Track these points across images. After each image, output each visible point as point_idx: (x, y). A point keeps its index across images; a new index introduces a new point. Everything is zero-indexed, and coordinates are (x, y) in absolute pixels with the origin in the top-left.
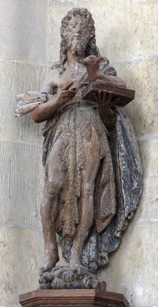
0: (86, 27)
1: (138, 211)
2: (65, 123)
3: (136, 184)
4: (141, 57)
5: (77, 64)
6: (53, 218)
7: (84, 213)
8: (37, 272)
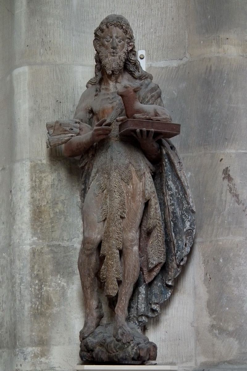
0: (123, 40)
3: (188, 224)
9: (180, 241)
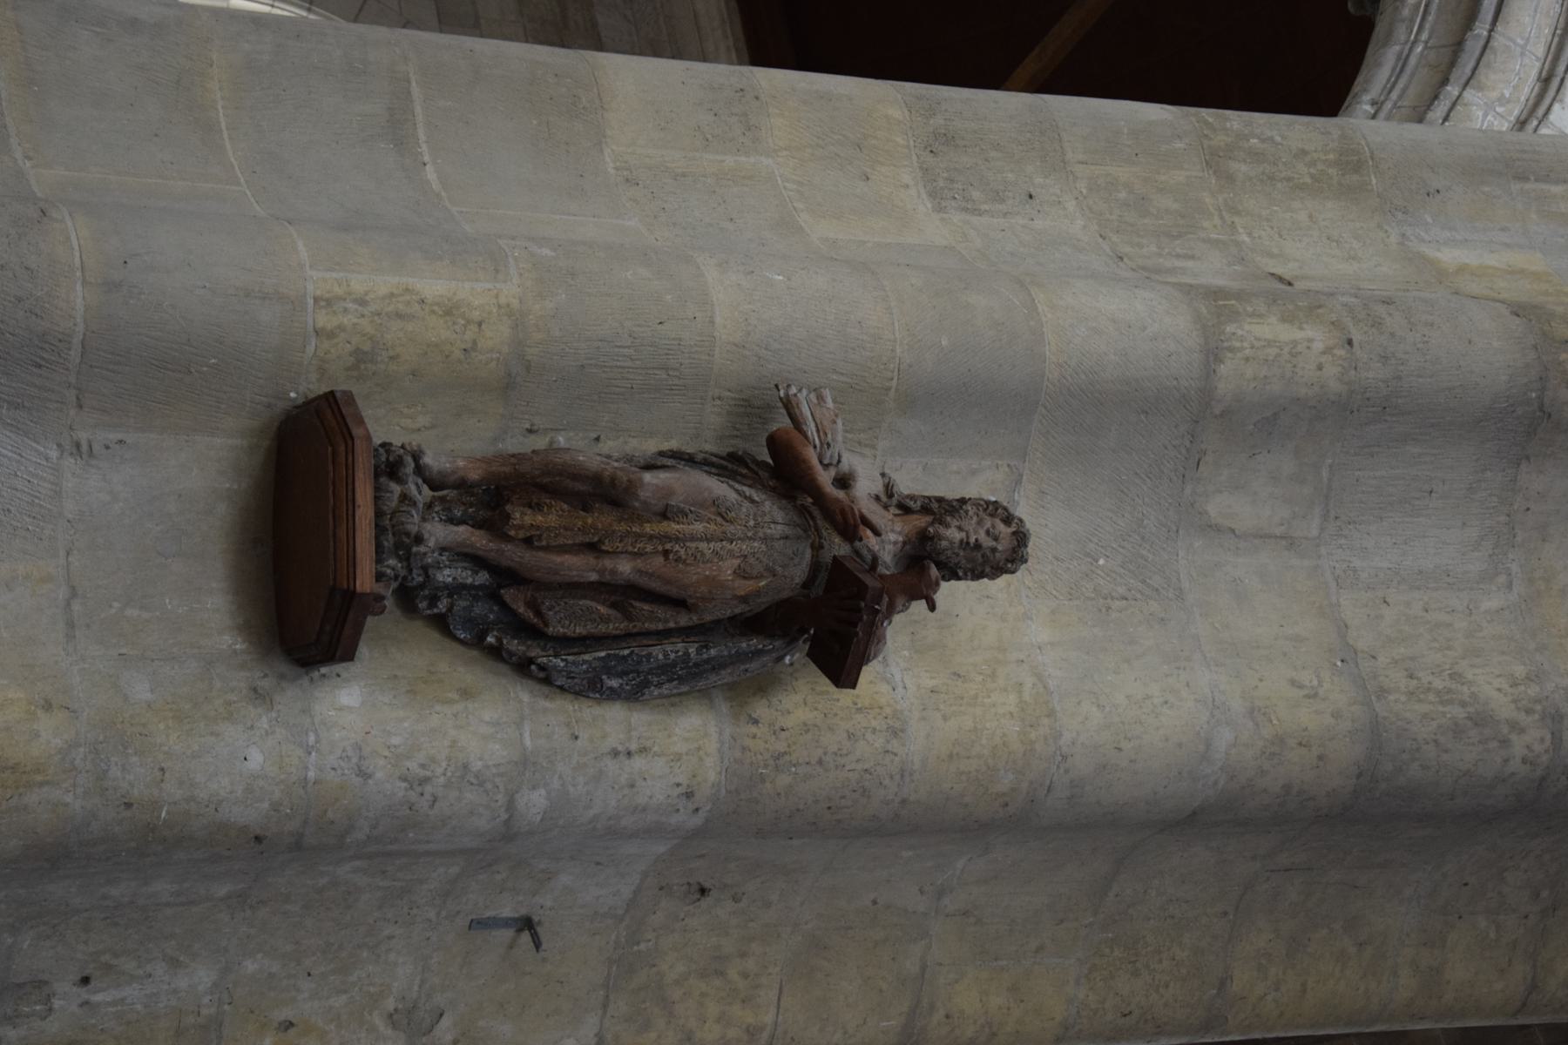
1: (546, 689)
2: (773, 516)
3: (614, 683)
4: (900, 689)
5: (901, 539)
6: (546, 480)
7: (558, 559)
8: (414, 440)
9: (588, 669)
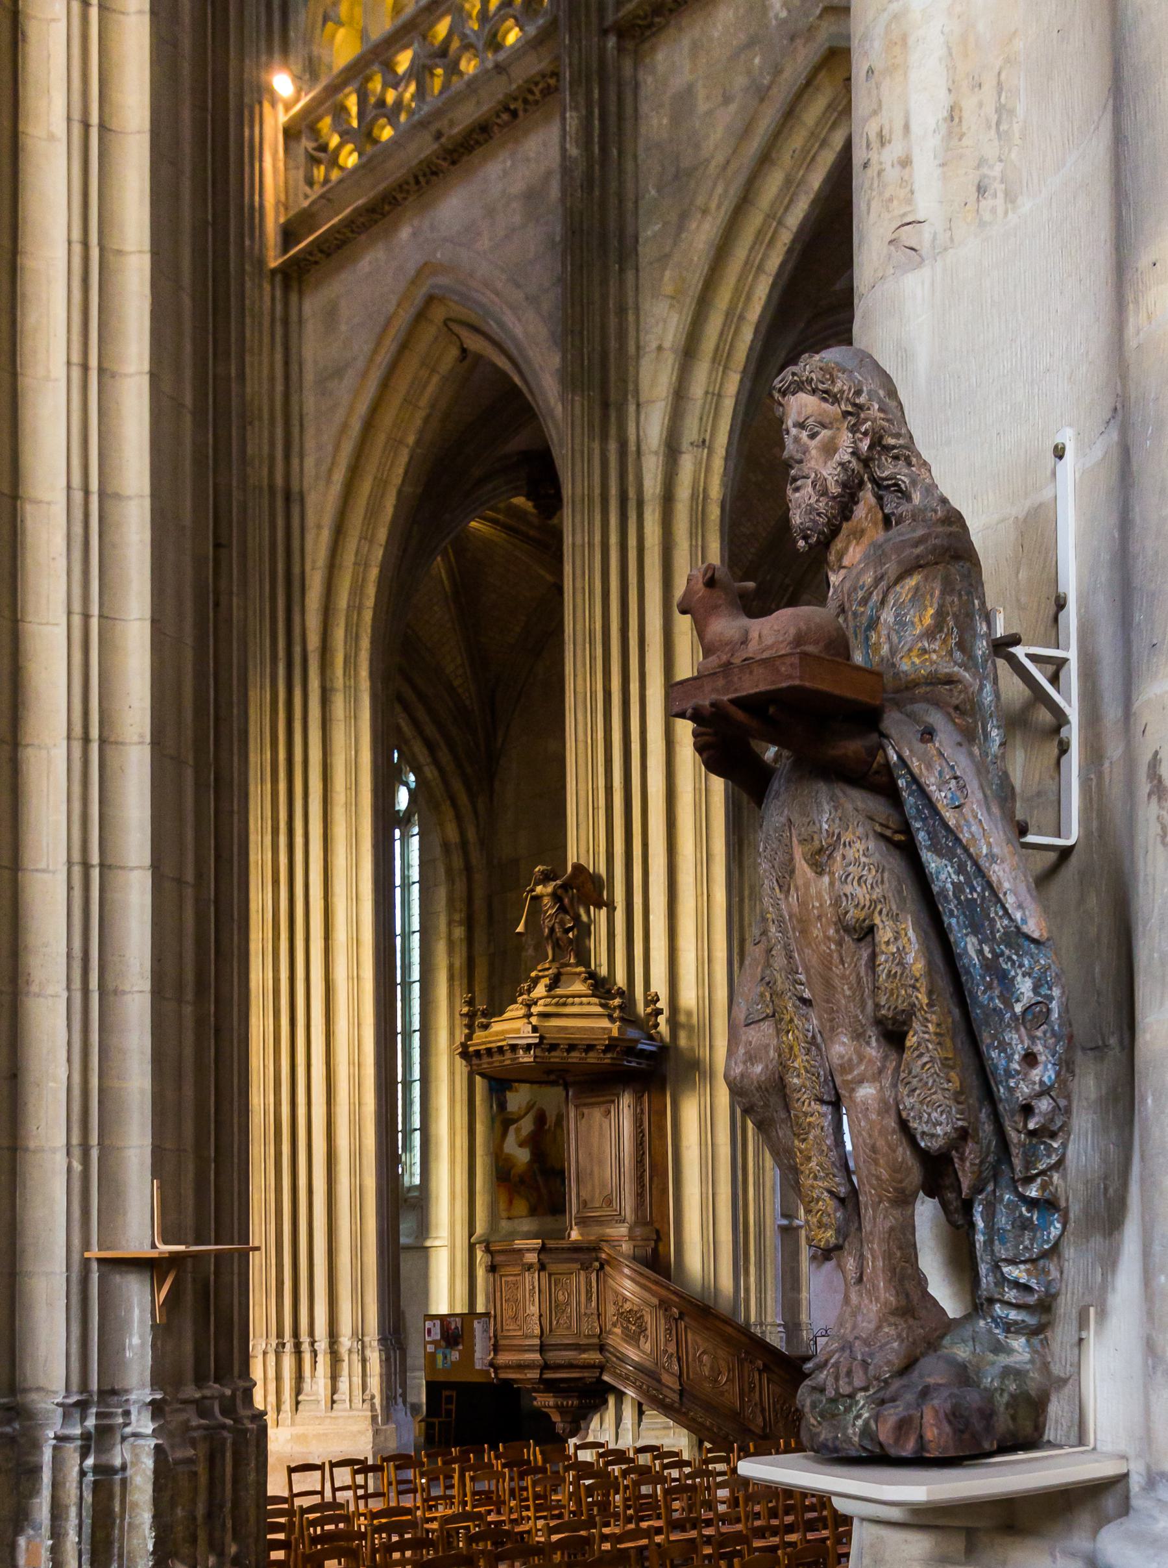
3: (1025, 986)
